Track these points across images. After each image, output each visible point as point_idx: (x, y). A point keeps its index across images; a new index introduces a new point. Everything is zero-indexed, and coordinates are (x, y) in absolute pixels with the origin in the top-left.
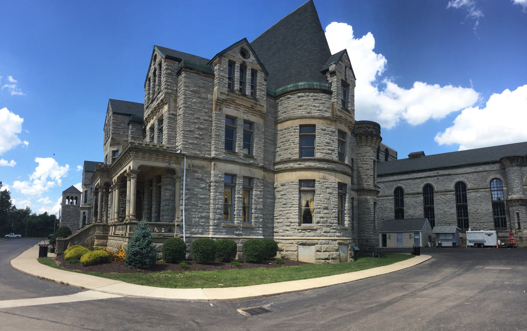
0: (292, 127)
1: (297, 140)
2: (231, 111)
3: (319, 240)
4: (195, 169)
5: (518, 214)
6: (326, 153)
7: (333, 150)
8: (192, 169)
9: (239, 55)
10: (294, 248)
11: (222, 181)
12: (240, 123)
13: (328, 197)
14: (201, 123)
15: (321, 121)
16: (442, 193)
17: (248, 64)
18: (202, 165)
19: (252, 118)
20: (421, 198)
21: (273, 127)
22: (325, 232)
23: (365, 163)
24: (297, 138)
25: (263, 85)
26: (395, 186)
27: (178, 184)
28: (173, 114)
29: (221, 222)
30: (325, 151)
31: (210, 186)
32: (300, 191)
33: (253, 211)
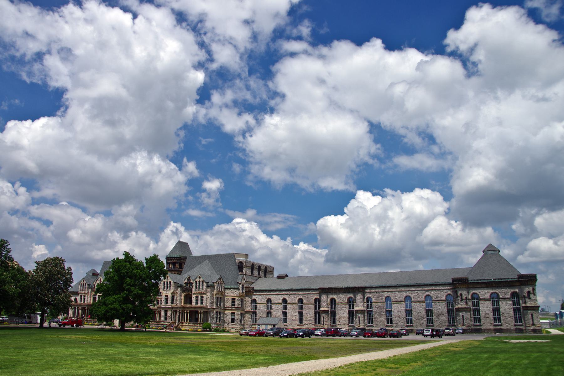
1: (231, 302)
2: (217, 296)
5: (323, 317)
10: (230, 329)
20: (280, 306)
32: (232, 315)
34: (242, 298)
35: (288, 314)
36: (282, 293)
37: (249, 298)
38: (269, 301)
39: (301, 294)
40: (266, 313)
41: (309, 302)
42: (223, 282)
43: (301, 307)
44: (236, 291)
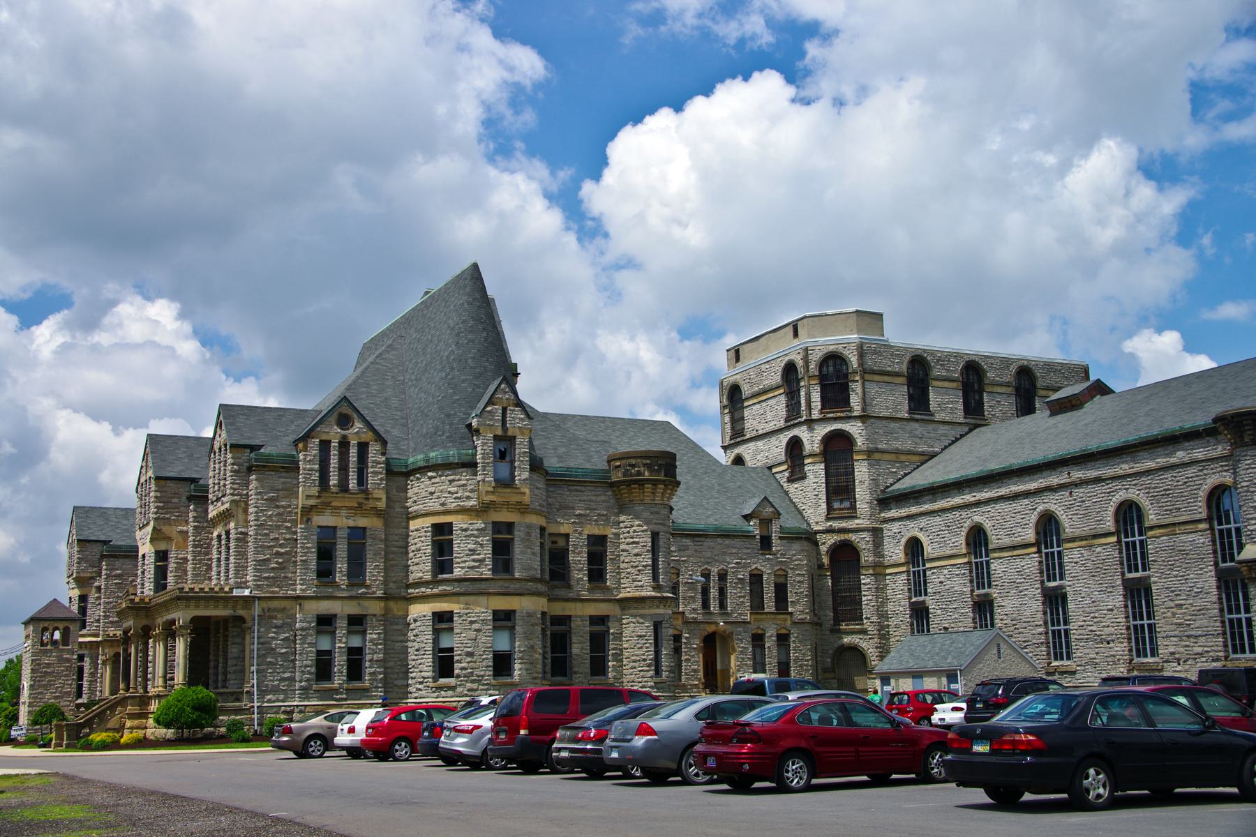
0: (423, 528)
2: (326, 520)
3: (459, 701)
4: (272, 614)
6: (469, 568)
7: (482, 561)
8: (267, 614)
9: (336, 427)
11: (313, 627)
12: (342, 534)
13: (474, 637)
14: (281, 546)
15: (460, 517)
16: (1084, 543)
17: (350, 437)
18: (282, 606)
19: (362, 522)
21: (404, 524)
22: (468, 690)
23: (632, 540)
24: (428, 545)
25: (380, 463)
26: (967, 524)
27: (248, 637)
28: (241, 533)
30: (467, 564)
31: (295, 636)
33: (367, 664)
34: (504, 516)
35: (1071, 606)
36: (1033, 486)
37: (637, 518)
38: (977, 538)
39: (1130, 475)
40: (968, 611)
41: (1176, 520)
42: (368, 436)
43: (1134, 557)
44: (451, 481)
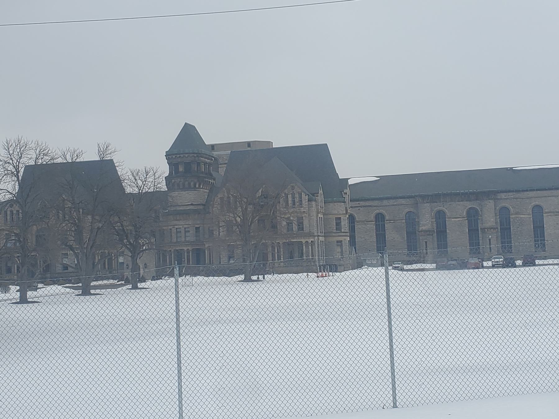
5: (426, 242)
29: (172, 180)
